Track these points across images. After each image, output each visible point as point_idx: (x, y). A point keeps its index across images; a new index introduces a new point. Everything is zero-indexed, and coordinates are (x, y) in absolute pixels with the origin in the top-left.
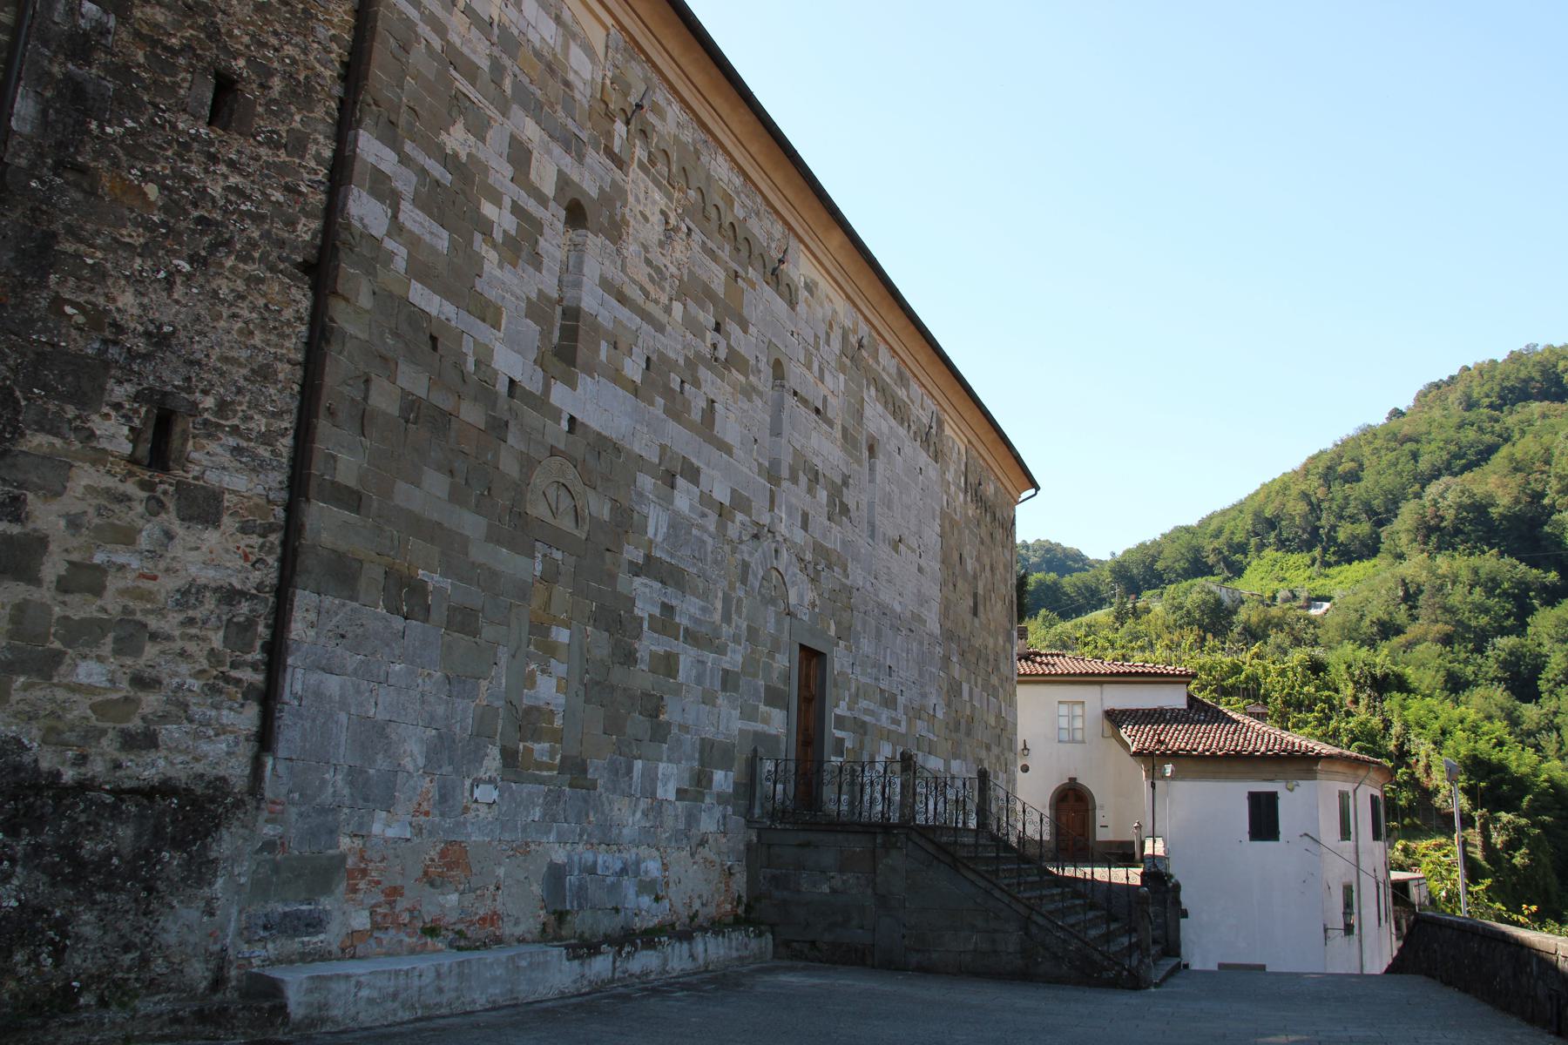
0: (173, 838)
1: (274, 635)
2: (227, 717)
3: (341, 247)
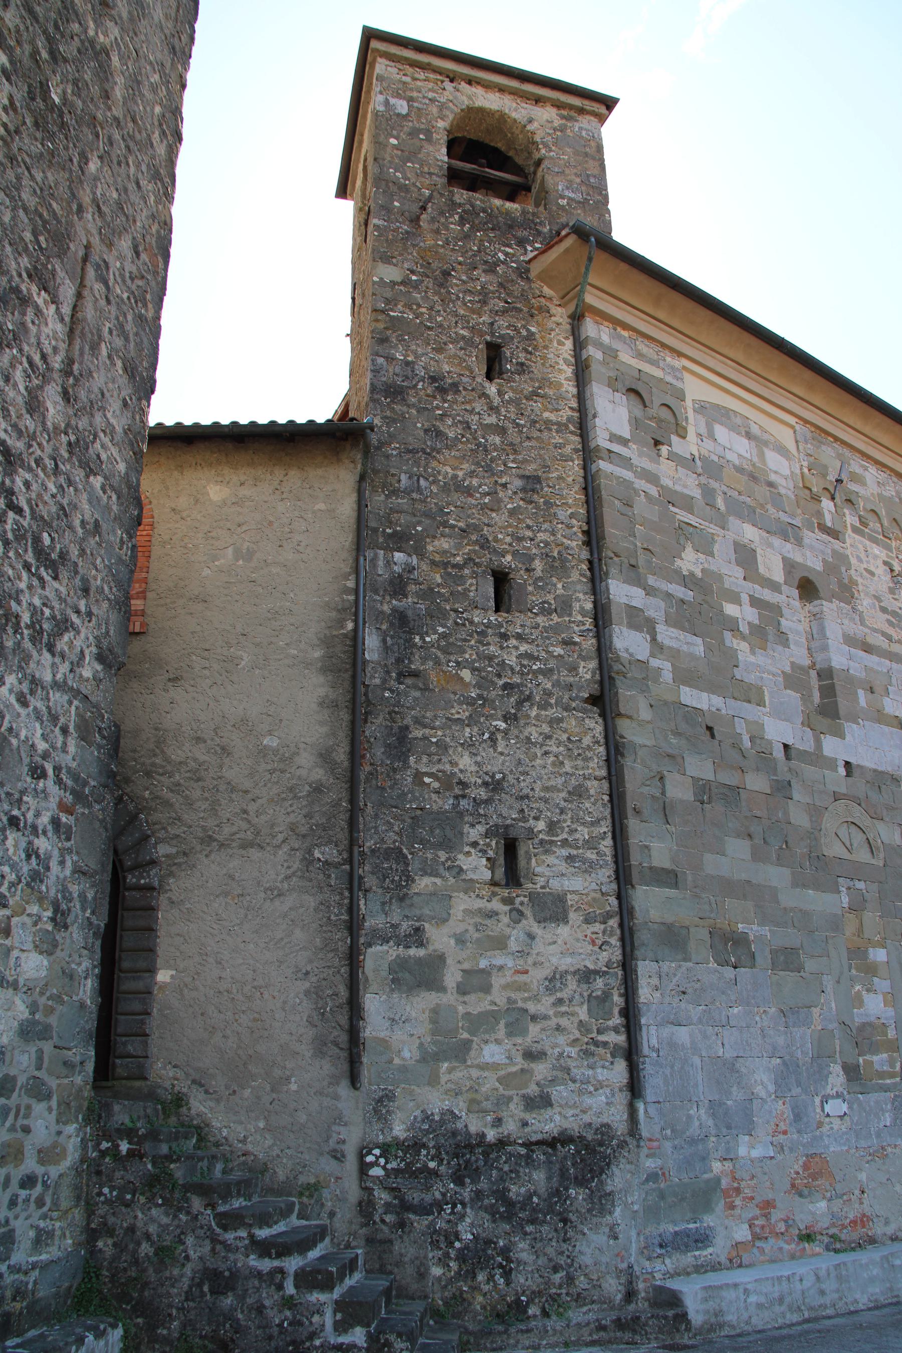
0: (576, 1178)
1: (627, 1002)
2: (602, 1074)
3: (616, 677)
